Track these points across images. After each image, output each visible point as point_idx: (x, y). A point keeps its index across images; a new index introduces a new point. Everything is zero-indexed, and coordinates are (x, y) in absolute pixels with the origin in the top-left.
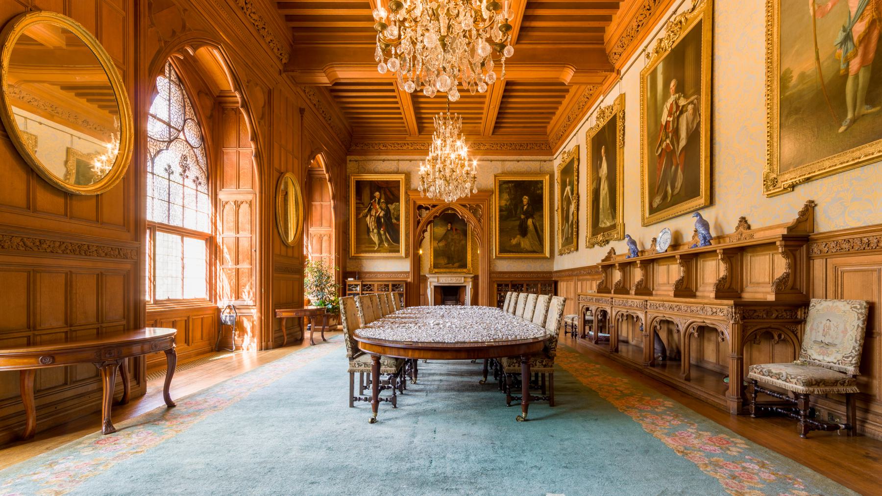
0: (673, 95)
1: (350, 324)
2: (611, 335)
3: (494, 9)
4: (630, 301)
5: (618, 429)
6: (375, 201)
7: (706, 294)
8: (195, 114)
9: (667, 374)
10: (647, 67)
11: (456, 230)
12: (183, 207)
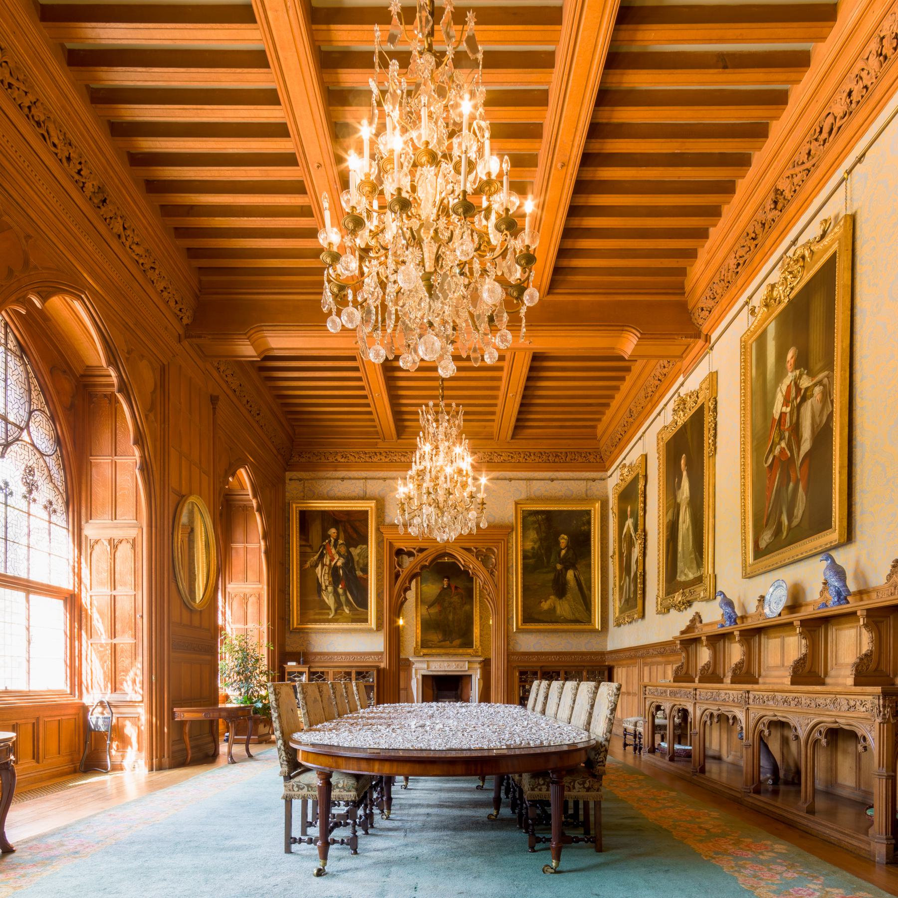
0: (792, 372)
1: (285, 725)
2: (694, 748)
3: (507, 229)
4: (723, 692)
5: (700, 885)
6: (330, 541)
7: (840, 681)
8: (47, 403)
9: (781, 805)
10: (752, 329)
11: (456, 588)
12: (29, 547)
